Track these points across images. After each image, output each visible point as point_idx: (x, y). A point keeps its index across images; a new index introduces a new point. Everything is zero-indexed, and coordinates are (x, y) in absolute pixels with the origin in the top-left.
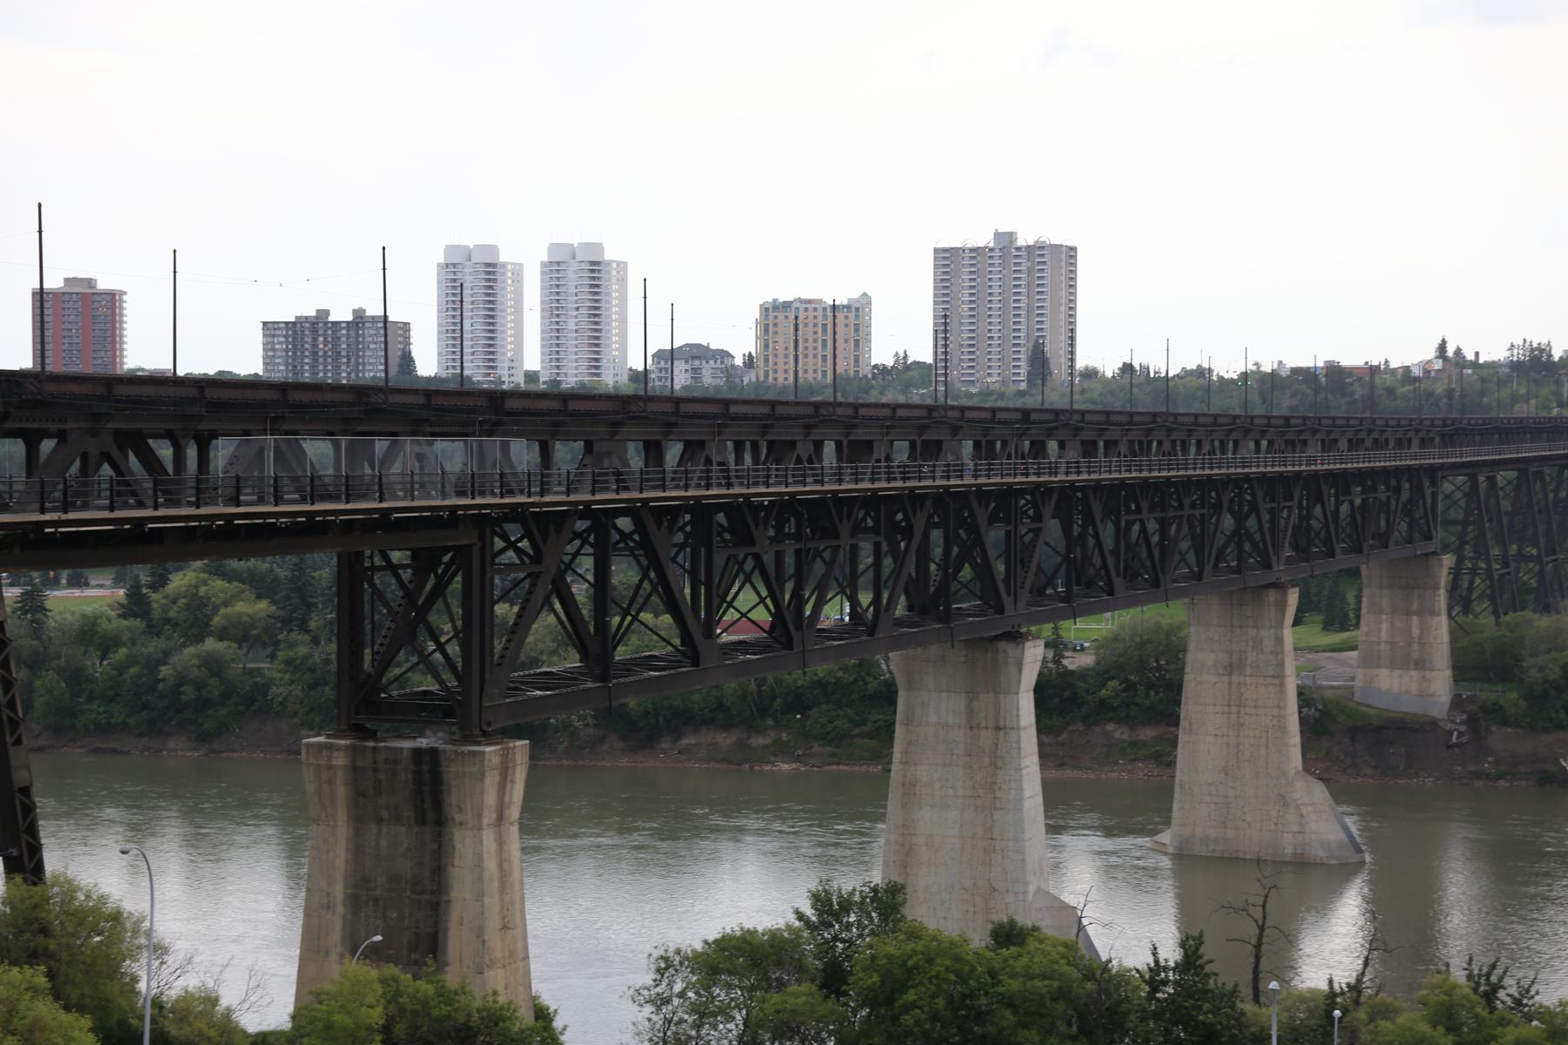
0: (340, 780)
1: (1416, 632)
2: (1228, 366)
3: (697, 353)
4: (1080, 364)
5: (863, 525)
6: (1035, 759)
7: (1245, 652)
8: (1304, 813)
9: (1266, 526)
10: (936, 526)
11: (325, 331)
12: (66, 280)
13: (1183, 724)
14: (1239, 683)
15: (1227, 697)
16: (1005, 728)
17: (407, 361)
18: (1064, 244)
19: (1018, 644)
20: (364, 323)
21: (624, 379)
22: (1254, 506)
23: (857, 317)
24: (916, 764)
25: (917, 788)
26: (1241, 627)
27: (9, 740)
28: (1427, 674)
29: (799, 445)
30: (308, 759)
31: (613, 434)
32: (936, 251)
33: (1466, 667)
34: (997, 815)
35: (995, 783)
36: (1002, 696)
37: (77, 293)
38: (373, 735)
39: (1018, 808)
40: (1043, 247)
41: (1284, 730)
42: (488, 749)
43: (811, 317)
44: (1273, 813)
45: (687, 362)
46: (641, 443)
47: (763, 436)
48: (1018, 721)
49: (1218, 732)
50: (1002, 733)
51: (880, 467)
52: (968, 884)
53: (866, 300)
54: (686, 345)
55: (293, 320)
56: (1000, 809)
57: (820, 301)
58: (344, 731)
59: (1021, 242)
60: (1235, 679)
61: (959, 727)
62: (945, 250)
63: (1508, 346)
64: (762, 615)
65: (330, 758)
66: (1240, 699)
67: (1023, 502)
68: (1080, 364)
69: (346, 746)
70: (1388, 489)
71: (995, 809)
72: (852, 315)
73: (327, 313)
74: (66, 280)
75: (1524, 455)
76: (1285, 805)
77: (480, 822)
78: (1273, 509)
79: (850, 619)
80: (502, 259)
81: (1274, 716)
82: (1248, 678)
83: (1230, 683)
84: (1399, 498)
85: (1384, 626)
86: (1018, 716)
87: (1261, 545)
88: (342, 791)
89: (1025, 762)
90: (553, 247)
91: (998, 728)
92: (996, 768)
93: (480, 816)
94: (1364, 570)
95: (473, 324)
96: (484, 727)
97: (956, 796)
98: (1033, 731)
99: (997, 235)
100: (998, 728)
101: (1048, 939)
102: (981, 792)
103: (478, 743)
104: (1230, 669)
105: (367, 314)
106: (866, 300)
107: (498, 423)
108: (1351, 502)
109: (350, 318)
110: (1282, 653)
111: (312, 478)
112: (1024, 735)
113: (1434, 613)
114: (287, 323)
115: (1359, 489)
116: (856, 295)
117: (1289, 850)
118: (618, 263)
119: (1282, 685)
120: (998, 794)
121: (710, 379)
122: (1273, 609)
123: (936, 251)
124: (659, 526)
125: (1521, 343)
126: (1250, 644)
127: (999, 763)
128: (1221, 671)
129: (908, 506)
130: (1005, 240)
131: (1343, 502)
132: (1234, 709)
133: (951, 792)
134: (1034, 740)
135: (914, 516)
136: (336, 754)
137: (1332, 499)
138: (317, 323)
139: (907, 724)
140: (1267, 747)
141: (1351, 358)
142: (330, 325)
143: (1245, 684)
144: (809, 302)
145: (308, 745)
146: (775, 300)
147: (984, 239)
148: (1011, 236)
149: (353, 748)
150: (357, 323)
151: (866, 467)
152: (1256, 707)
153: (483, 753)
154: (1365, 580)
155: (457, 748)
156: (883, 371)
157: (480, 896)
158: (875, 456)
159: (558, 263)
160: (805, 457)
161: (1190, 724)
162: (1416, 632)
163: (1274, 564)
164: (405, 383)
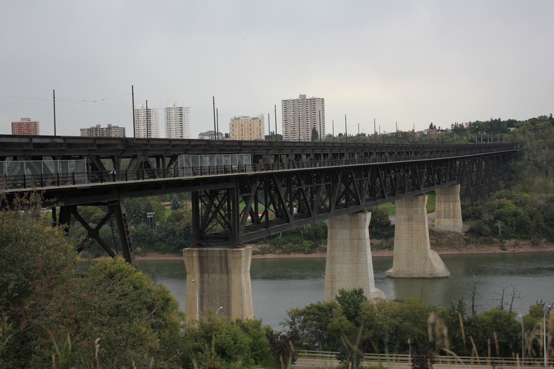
1: (452, 207)
5: (260, 187)
7: (413, 215)
8: (432, 261)
10: (261, 189)
11: (100, 131)
12: (22, 119)
13: (395, 237)
14: (412, 224)
15: (408, 228)
16: (361, 239)
18: (321, 98)
19: (365, 214)
20: (111, 128)
22: (352, 179)
24: (334, 251)
25: (335, 258)
26: (412, 207)
27: (130, 250)
28: (455, 220)
29: (311, 155)
30: (185, 255)
31: (267, 152)
35: (359, 256)
36: (360, 230)
37: (25, 123)
38: (203, 246)
39: (366, 264)
40: (314, 99)
41: (425, 237)
42: (242, 249)
43: (246, 122)
44: (423, 262)
45: (209, 136)
46: (274, 156)
47: (303, 152)
48: (365, 237)
49: (406, 239)
50: (360, 241)
51: (330, 161)
54: (209, 131)
55: (90, 128)
56: (361, 263)
57: (249, 117)
58: (195, 246)
59: (308, 98)
60: (410, 223)
61: (347, 239)
63: (451, 125)
65: (192, 254)
66: (412, 229)
67: (294, 178)
69: (197, 250)
70: (404, 171)
71: (359, 263)
73: (100, 126)
75: (432, 159)
77: (241, 272)
78: (360, 180)
79: (298, 211)
81: (422, 233)
82: (414, 222)
83: (409, 224)
84: (408, 174)
85: (442, 206)
86: (365, 235)
89: (367, 249)
92: (359, 251)
93: (240, 270)
94: (436, 191)
96: (239, 243)
97: (347, 260)
99: (300, 96)
100: (359, 239)
102: (355, 259)
103: (239, 248)
104: (409, 220)
105: (112, 125)
107: (241, 150)
108: (391, 176)
109: (107, 127)
110: (424, 214)
111: (201, 167)
113: (456, 202)
114: (88, 129)
115: (393, 171)
117: (428, 273)
119: (424, 224)
120: (360, 259)
122: (421, 202)
124: (279, 181)
125: (455, 124)
126: (415, 212)
127: (360, 250)
128: (406, 221)
129: (249, 183)
130: (303, 97)
131: (387, 176)
132: (410, 232)
133: (345, 259)
135: (252, 186)
136: (194, 253)
137: (383, 175)
138: (97, 129)
139: (331, 239)
140: (421, 242)
142: (101, 129)
143: (414, 224)
145: (185, 250)
147: (296, 97)
148: (304, 96)
150: (109, 128)
152: (417, 231)
153: (241, 251)
154: (436, 193)
155: (232, 249)
157: (241, 294)
158: (329, 158)
160: (312, 159)
161: (398, 236)
162: (452, 207)
163: (421, 188)
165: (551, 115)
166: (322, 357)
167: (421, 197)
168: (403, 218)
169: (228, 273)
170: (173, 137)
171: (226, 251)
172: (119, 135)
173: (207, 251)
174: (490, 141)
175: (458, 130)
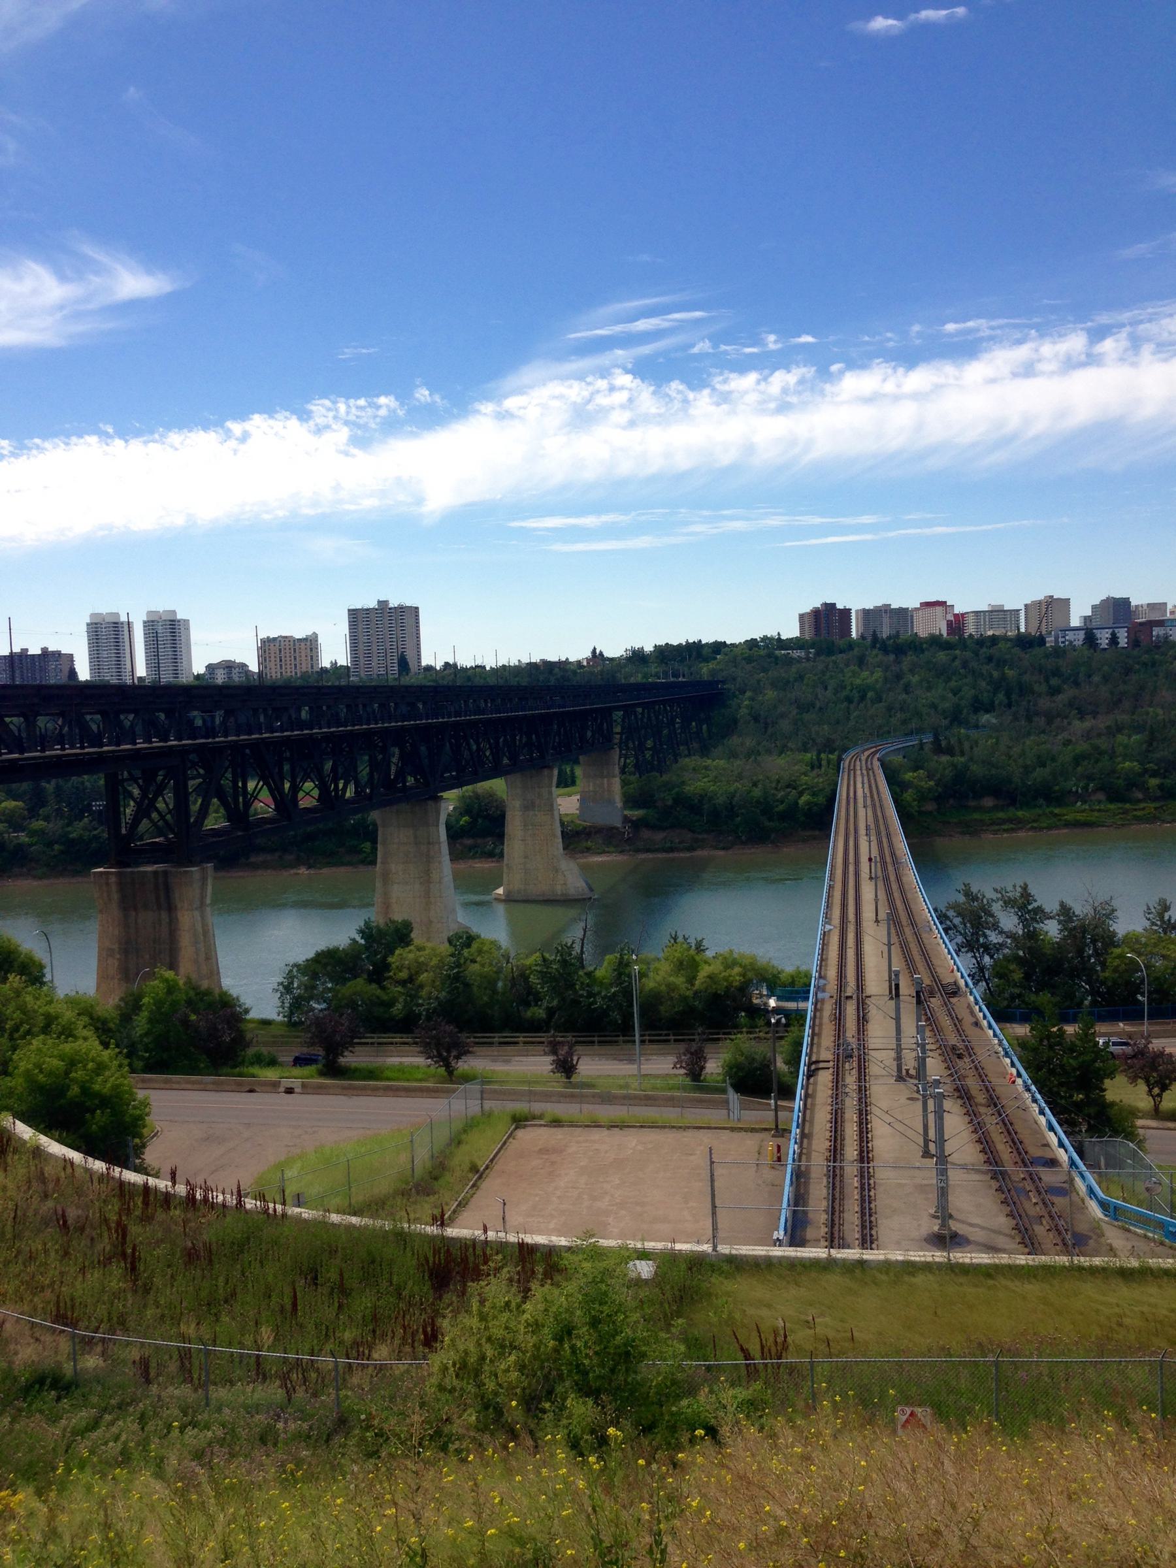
0: (114, 888)
1: (606, 785)
2: (490, 663)
3: (229, 666)
4: (424, 663)
6: (448, 857)
17: (73, 673)
21: (192, 679)
23: (311, 644)
33: (631, 801)
53: (315, 636)
59: (391, 605)
62: (353, 610)
64: (316, 793)
68: (424, 663)
72: (308, 643)
73: (27, 650)
80: (179, 617)
88: (115, 896)
91: (429, 843)
95: (165, 652)
98: (446, 843)
99: (379, 602)
100: (429, 843)
101: (292, 907)
112: (442, 845)
117: (559, 892)
118: (185, 620)
121: (237, 678)
130: (383, 604)
134: (447, 847)
141: (553, 658)
144: (286, 637)
147: (372, 604)
148: (386, 602)
149: (118, 874)
153: (192, 871)
156: (324, 671)
159: (153, 621)
162: (606, 785)
164: (72, 683)
165: (779, 634)
166: (379, 1044)
167: (546, 772)
168: (518, 806)
169: (171, 908)
170: (164, 681)
171: (165, 873)
172: (60, 679)
173: (132, 873)
174: (684, 676)
175: (637, 657)
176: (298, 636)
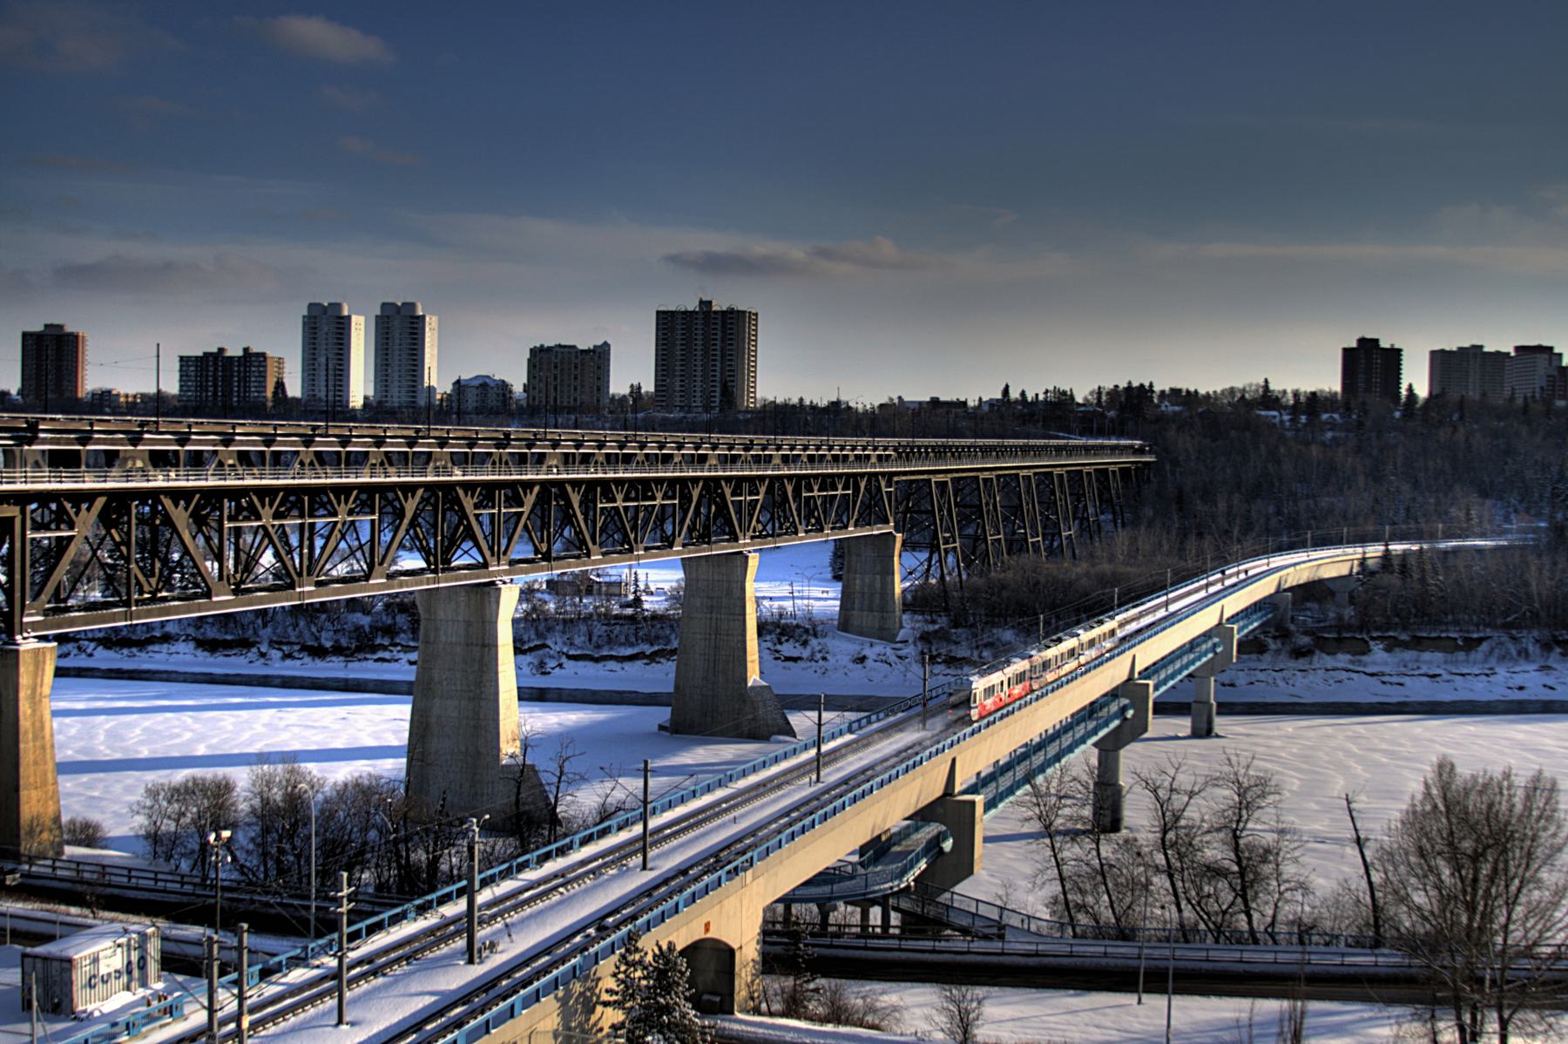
1: (878, 585)
9: (256, 545)
12: (46, 326)
32: (658, 313)
34: (483, 703)
52: (463, 749)
74: (46, 326)
76: (744, 701)
87: (318, 551)
90: (311, 306)
91: (484, 646)
99: (701, 302)
100: (484, 646)
106: (606, 345)
109: (240, 353)
116: (599, 343)
123: (658, 313)
146: (542, 346)
151: (115, 472)
176: (581, 347)
